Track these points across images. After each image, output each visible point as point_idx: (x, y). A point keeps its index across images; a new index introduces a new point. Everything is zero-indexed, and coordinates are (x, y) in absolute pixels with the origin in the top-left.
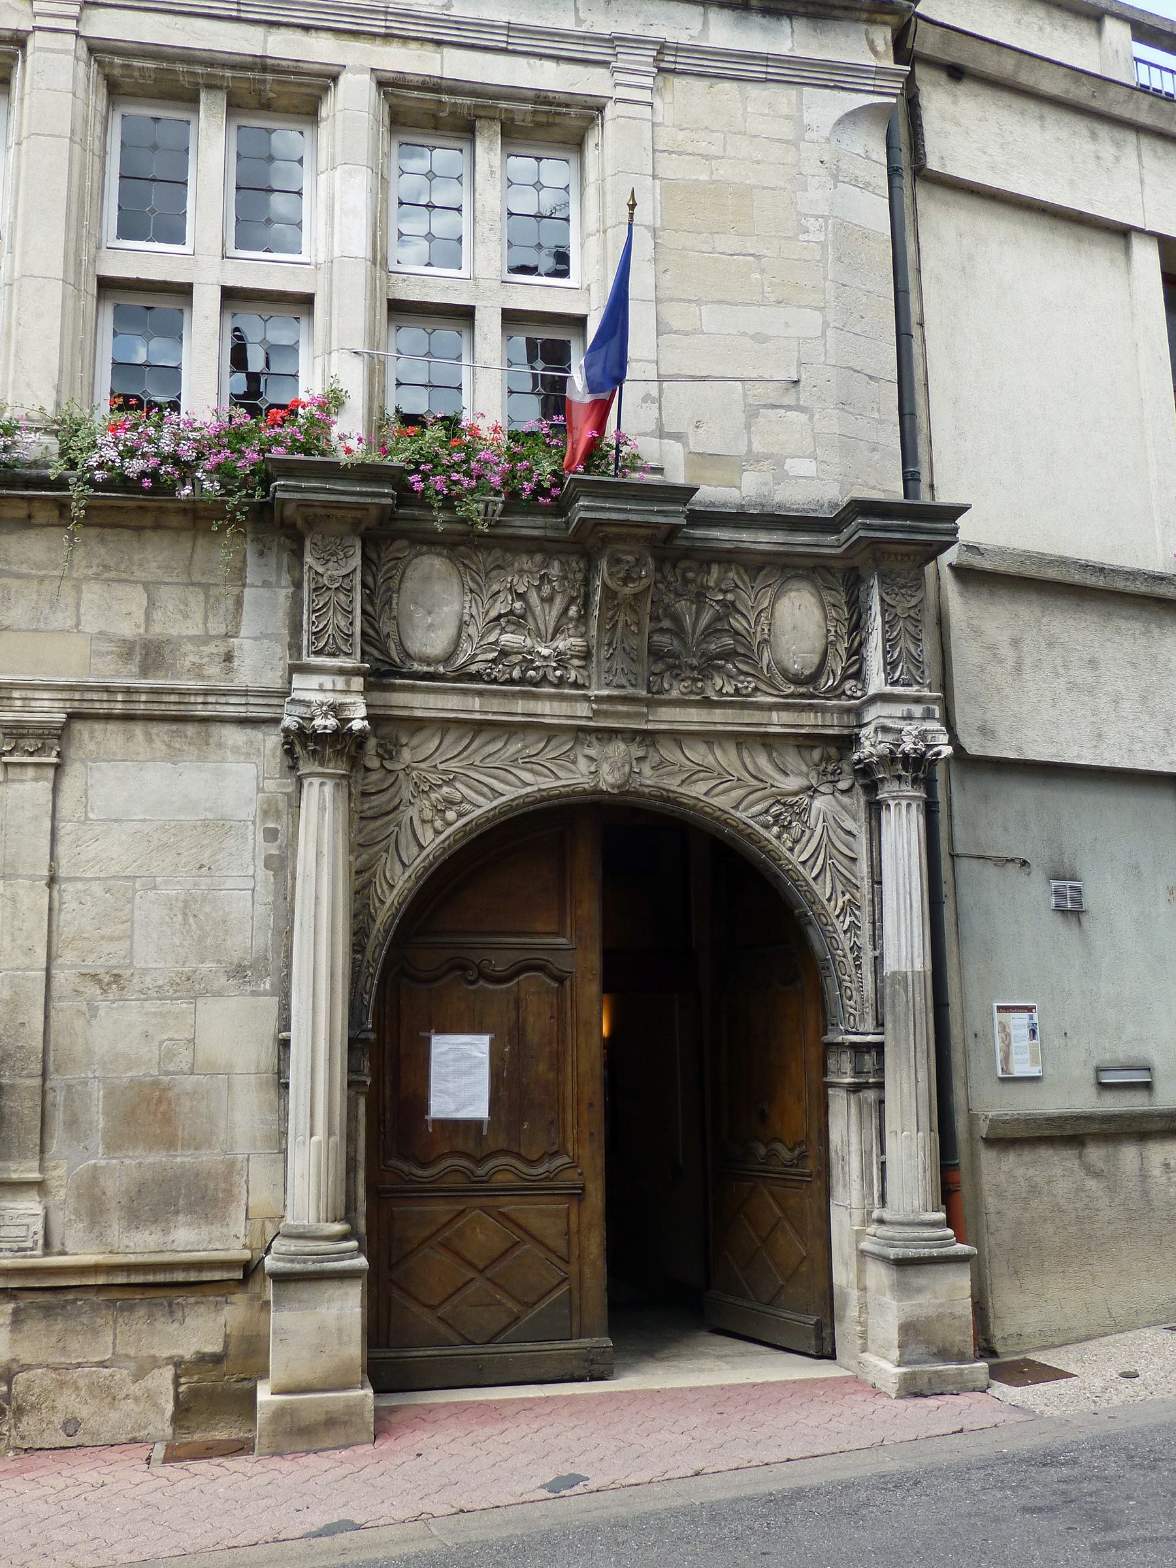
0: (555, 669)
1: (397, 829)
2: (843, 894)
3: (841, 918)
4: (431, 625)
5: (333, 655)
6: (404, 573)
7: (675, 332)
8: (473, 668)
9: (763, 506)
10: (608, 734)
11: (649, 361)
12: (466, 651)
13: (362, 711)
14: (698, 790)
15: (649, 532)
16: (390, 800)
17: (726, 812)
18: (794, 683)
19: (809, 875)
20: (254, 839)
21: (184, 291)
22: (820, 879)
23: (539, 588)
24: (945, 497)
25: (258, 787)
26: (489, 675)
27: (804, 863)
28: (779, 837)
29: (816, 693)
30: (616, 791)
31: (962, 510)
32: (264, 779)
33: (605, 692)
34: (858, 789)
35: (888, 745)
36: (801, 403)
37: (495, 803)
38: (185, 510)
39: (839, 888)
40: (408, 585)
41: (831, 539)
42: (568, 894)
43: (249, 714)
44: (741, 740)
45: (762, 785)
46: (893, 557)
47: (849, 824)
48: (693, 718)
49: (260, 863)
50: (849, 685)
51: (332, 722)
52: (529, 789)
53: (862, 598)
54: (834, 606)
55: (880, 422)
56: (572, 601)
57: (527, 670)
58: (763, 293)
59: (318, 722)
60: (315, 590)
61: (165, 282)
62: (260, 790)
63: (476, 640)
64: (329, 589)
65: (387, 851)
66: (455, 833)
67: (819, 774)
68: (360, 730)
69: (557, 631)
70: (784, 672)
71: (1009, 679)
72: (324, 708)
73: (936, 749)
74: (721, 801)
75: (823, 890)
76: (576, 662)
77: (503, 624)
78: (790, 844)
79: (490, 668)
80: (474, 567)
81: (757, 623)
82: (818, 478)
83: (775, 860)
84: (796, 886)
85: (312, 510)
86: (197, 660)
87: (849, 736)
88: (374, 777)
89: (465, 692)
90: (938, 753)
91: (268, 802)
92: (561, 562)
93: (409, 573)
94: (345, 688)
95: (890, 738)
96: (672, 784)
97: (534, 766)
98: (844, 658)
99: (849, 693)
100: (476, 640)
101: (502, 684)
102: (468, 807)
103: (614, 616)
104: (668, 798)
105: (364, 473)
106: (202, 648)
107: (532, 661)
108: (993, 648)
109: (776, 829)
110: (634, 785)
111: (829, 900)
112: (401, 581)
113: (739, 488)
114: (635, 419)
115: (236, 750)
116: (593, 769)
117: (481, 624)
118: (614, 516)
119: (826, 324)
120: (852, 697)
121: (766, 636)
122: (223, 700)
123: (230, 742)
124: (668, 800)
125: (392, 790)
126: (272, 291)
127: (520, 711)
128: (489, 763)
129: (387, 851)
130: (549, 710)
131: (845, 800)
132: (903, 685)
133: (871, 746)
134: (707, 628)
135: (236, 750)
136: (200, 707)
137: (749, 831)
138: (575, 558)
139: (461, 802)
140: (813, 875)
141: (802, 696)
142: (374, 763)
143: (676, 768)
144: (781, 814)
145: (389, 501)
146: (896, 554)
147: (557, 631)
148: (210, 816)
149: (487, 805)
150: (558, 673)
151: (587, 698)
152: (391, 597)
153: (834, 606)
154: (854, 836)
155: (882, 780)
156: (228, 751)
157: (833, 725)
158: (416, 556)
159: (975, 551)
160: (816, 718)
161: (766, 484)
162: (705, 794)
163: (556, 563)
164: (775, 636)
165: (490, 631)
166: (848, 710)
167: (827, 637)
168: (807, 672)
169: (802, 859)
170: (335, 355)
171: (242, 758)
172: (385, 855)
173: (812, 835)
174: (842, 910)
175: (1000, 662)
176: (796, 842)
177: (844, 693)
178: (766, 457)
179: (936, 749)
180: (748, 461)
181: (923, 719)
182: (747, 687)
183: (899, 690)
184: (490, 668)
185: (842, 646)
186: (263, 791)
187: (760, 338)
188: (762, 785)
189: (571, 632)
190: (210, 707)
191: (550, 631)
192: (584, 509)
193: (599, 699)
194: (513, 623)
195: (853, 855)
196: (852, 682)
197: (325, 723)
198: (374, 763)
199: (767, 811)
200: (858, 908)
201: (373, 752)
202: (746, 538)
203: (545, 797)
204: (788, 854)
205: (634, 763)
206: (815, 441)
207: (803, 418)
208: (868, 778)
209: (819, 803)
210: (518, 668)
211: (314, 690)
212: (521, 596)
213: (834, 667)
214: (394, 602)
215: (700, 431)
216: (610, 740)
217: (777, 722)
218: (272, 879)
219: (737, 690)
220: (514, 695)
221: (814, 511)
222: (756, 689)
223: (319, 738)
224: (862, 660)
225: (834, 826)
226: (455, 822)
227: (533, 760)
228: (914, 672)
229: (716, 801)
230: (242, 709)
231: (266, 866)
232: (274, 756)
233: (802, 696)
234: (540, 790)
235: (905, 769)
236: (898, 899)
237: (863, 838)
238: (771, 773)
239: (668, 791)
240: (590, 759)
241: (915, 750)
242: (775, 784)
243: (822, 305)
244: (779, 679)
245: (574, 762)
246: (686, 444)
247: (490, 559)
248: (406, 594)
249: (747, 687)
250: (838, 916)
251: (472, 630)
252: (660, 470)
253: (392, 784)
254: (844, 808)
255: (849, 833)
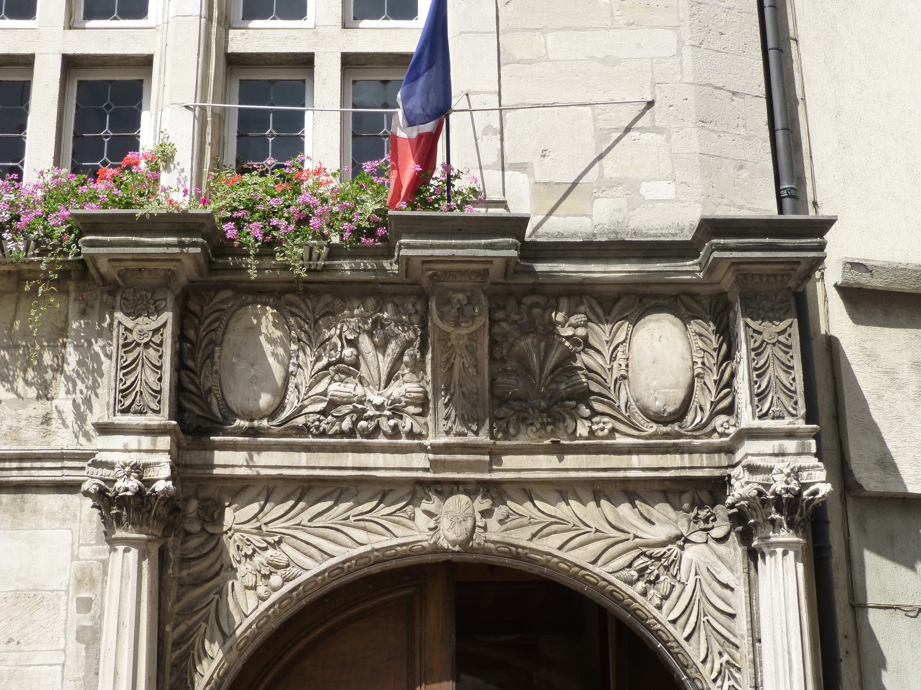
0: (389, 418)
1: (217, 596)
2: (721, 654)
3: (719, 682)
4: (255, 377)
5: (141, 413)
6: (227, 324)
7: (518, 62)
8: (300, 421)
9: (617, 233)
10: (445, 489)
11: (490, 93)
12: (293, 403)
13: (166, 471)
14: (550, 544)
15: (481, 267)
16: (212, 565)
17: (582, 568)
18: (657, 422)
19: (681, 636)
20: (67, 610)
21: (306, 61)
22: (694, 638)
23: (371, 335)
24: (825, 212)
25: (72, 554)
26: (317, 428)
27: (674, 622)
28: (644, 594)
29: (682, 431)
30: (457, 548)
31: (828, 223)
32: (80, 545)
33: (443, 440)
34: (733, 537)
35: (756, 486)
36: (657, 124)
37: (325, 566)
38: (9, 273)
39: (716, 648)
40: (230, 336)
41: (689, 265)
42: (417, 661)
43: (65, 478)
44: (599, 490)
45: (623, 536)
46: (757, 279)
47: (725, 576)
48: (542, 465)
49: (72, 636)
50: (721, 419)
51: (133, 484)
52: (362, 550)
53: (731, 327)
54: (700, 335)
55: (748, 138)
56: (409, 344)
57: (359, 419)
58: (612, 16)
59: (120, 484)
60: (124, 346)
61: (9, 56)
62: (75, 557)
63: (303, 390)
64: (138, 345)
65: (206, 621)
66: (280, 600)
67: (689, 521)
68: (163, 492)
69: (391, 376)
70: (645, 411)
71: (912, 405)
72: (127, 469)
73: (812, 488)
74: (579, 556)
75: (695, 651)
76: (411, 409)
77: (332, 373)
78: (658, 601)
79: (319, 420)
80: (302, 315)
81: (613, 359)
82: (678, 200)
83: (642, 619)
84: (668, 648)
85: (123, 264)
86: (15, 424)
87: (722, 478)
88: (194, 542)
89: (290, 448)
90: (815, 493)
91: (83, 570)
92: (396, 305)
93: (232, 324)
94: (151, 448)
95: (759, 478)
96: (521, 538)
97: (367, 524)
98: (714, 391)
99: (720, 430)
100: (303, 390)
101: (332, 436)
102: (293, 570)
103: (448, 360)
104: (516, 553)
105: (177, 223)
106: (20, 412)
107: (364, 411)
108: (890, 373)
109: (641, 585)
110: (479, 538)
111: (704, 661)
112: (224, 333)
113: (590, 216)
114: (468, 154)
115: (51, 516)
116: (432, 525)
117: (307, 372)
118: (438, 252)
119: (680, 42)
120: (722, 435)
121: (624, 372)
122: (38, 464)
123: (45, 508)
124: (517, 557)
125: (213, 555)
126: (113, 56)
127: (350, 465)
128: (318, 522)
129: (206, 621)
130: (383, 464)
131: (721, 548)
132: (773, 418)
133: (742, 487)
134: (556, 367)
135: (51, 516)
136: (14, 473)
137: (611, 588)
138: (412, 299)
139: (288, 566)
140: (686, 634)
141: (667, 435)
142: (195, 527)
143: (525, 520)
144: (647, 568)
145: (514, 253)
146: (760, 275)
147: (391, 376)
148: (22, 586)
149: (315, 568)
150: (392, 422)
151: (423, 449)
152: (213, 351)
153: (700, 335)
154: (732, 589)
155: (755, 525)
156: (44, 518)
157: (701, 466)
158: (241, 306)
159: (863, 269)
160: (682, 459)
161: (620, 210)
162: (560, 548)
163: (390, 306)
164: (633, 371)
165: (318, 381)
166: (719, 449)
167: (693, 370)
168: (670, 409)
169: (673, 616)
170: (167, 111)
171: (57, 524)
172: (204, 625)
173: (683, 590)
174: (720, 673)
175: (899, 388)
176: (665, 598)
177: (714, 430)
178: (619, 182)
179: (812, 488)
180: (599, 188)
181: (798, 454)
182: (603, 429)
183: (768, 424)
184: (319, 420)
185: (711, 379)
186: (79, 559)
187: (610, 61)
188: (623, 536)
189: (406, 378)
190: (25, 473)
191: (384, 378)
192: (411, 248)
193: (436, 449)
194: (343, 372)
195: (731, 611)
196: (723, 418)
197: (128, 485)
198: (195, 527)
199: (630, 566)
200: (739, 669)
201: (193, 515)
202: (597, 270)
203: (382, 556)
204: (656, 612)
205: (478, 516)
206: (673, 162)
207: (660, 139)
208: (746, 526)
209: (690, 554)
210: (348, 418)
211: (119, 451)
212: (353, 343)
213: (703, 403)
214: (217, 355)
215: (547, 159)
216: (452, 493)
217: (638, 466)
218: (84, 653)
219: (592, 433)
220: (343, 449)
221: (673, 235)
222: (613, 430)
223: (122, 502)
224: (733, 393)
225: (709, 579)
226: (279, 587)
227: (365, 517)
228: (786, 403)
229: (572, 556)
230: (58, 473)
231: (78, 639)
232: (90, 521)
233: (667, 435)
234: (373, 550)
235: (779, 511)
236: (776, 659)
237: (741, 590)
238: (635, 522)
239: (517, 547)
240: (430, 514)
241: (787, 491)
242: (639, 534)
243: (676, 24)
244: (639, 419)
245: (412, 519)
246: (531, 175)
247: (321, 305)
248: (227, 348)
249: (603, 429)
250: (715, 681)
251: (299, 379)
252: (503, 204)
253: (213, 549)
254: (720, 557)
255: (726, 586)
